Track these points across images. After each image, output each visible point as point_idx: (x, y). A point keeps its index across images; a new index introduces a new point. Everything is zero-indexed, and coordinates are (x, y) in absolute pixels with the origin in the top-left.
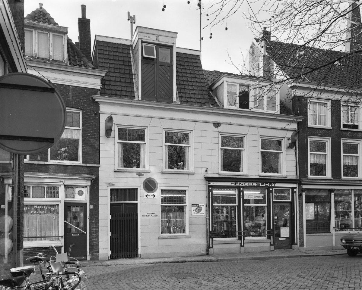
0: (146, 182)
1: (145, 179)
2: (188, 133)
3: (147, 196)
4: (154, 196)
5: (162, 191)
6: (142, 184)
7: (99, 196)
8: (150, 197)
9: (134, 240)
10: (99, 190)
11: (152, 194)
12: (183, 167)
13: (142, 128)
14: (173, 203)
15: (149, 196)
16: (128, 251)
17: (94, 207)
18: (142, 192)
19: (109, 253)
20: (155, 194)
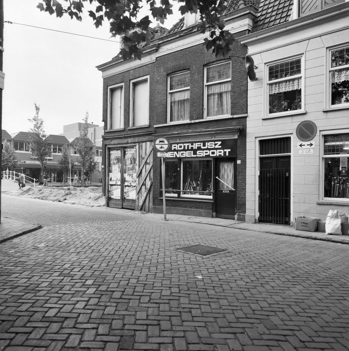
0: (301, 128)
1: (299, 123)
2: (300, 58)
3: (301, 145)
4: (311, 145)
5: (325, 136)
6: (295, 130)
7: (247, 149)
8: (306, 147)
9: (269, 203)
10: (247, 143)
11: (309, 143)
12: (299, 107)
13: (294, 59)
14: (330, 153)
15: (304, 145)
16: (265, 215)
17: (241, 161)
18: (295, 142)
19: (258, 215)
20: (312, 142)
